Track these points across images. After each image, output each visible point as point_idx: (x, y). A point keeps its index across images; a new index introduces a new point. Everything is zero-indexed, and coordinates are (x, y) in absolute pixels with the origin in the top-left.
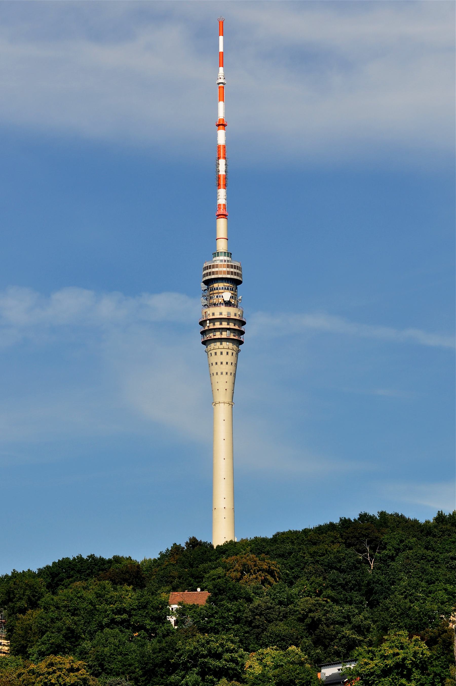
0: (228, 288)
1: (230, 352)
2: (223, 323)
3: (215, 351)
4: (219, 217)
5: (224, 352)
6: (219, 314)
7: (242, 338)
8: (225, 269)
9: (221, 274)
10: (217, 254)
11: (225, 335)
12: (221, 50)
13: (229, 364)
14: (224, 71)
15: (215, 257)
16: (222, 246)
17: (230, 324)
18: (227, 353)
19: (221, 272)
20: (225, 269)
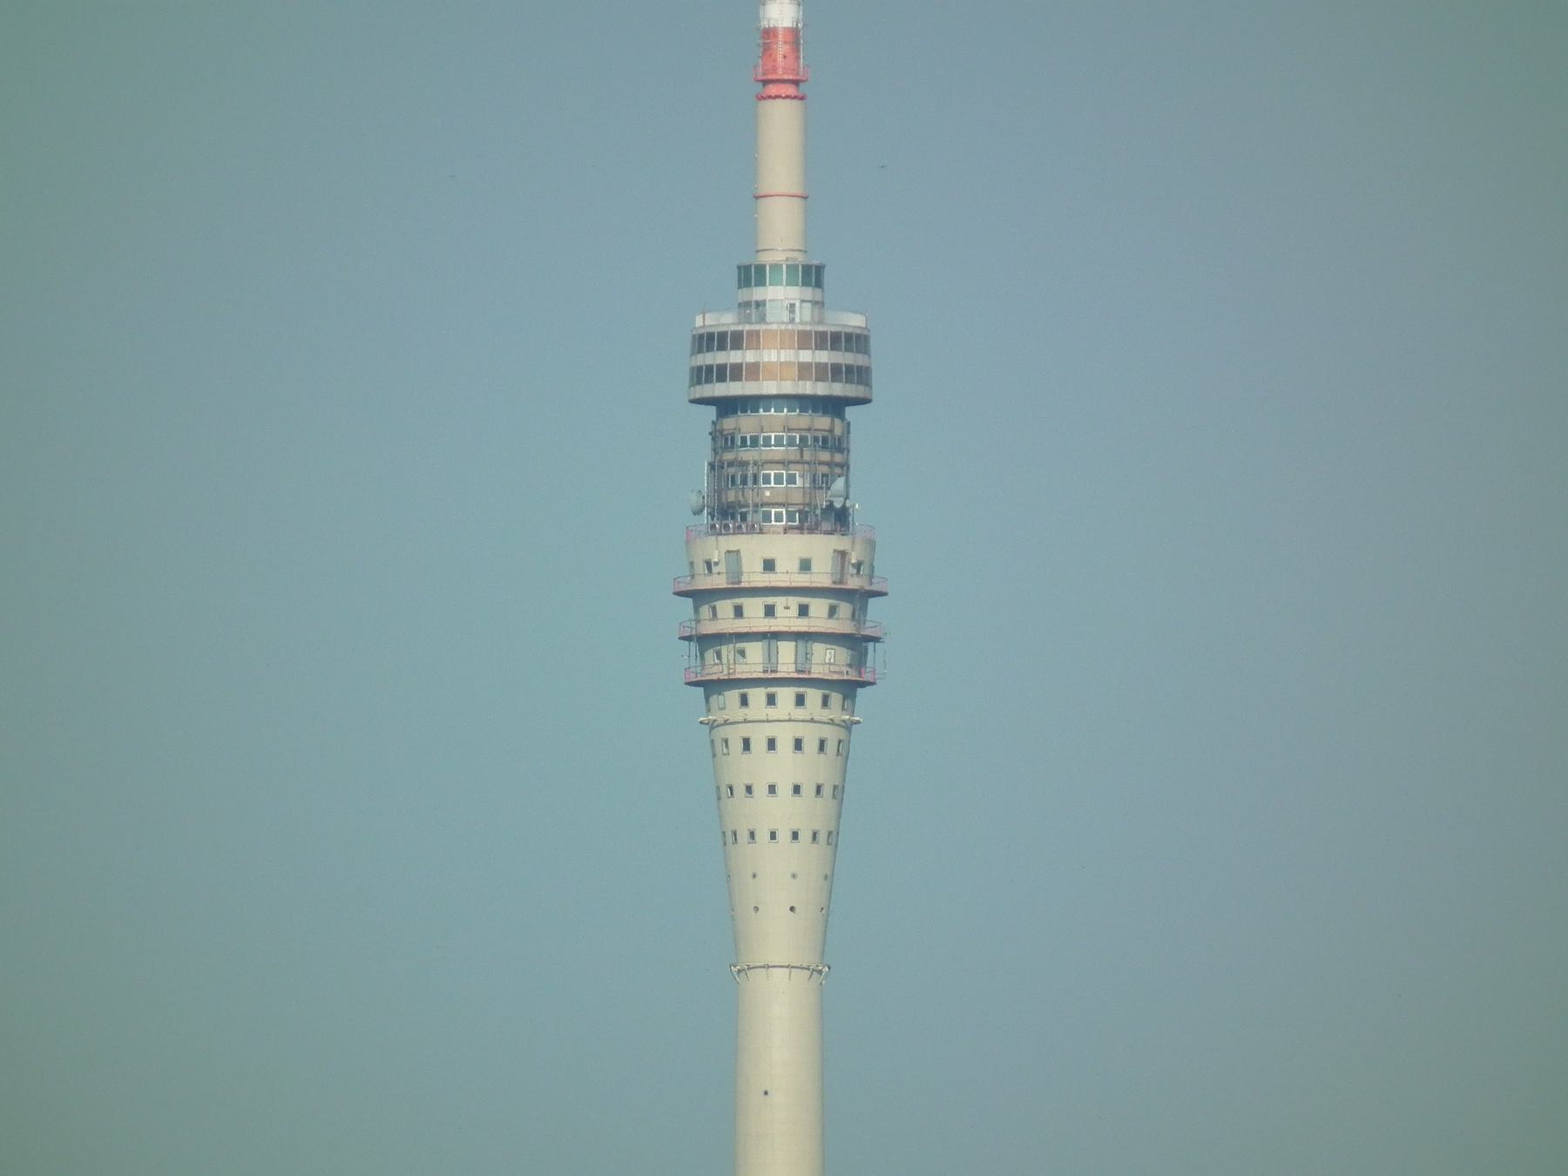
0: (803, 439)
3: (745, 731)
4: (773, 89)
6: (796, 566)
7: (803, 88)
8: (787, 355)
10: (751, 275)
14: (810, 131)
16: (781, 233)
18: (798, 744)
19: (775, 371)
20: (787, 355)
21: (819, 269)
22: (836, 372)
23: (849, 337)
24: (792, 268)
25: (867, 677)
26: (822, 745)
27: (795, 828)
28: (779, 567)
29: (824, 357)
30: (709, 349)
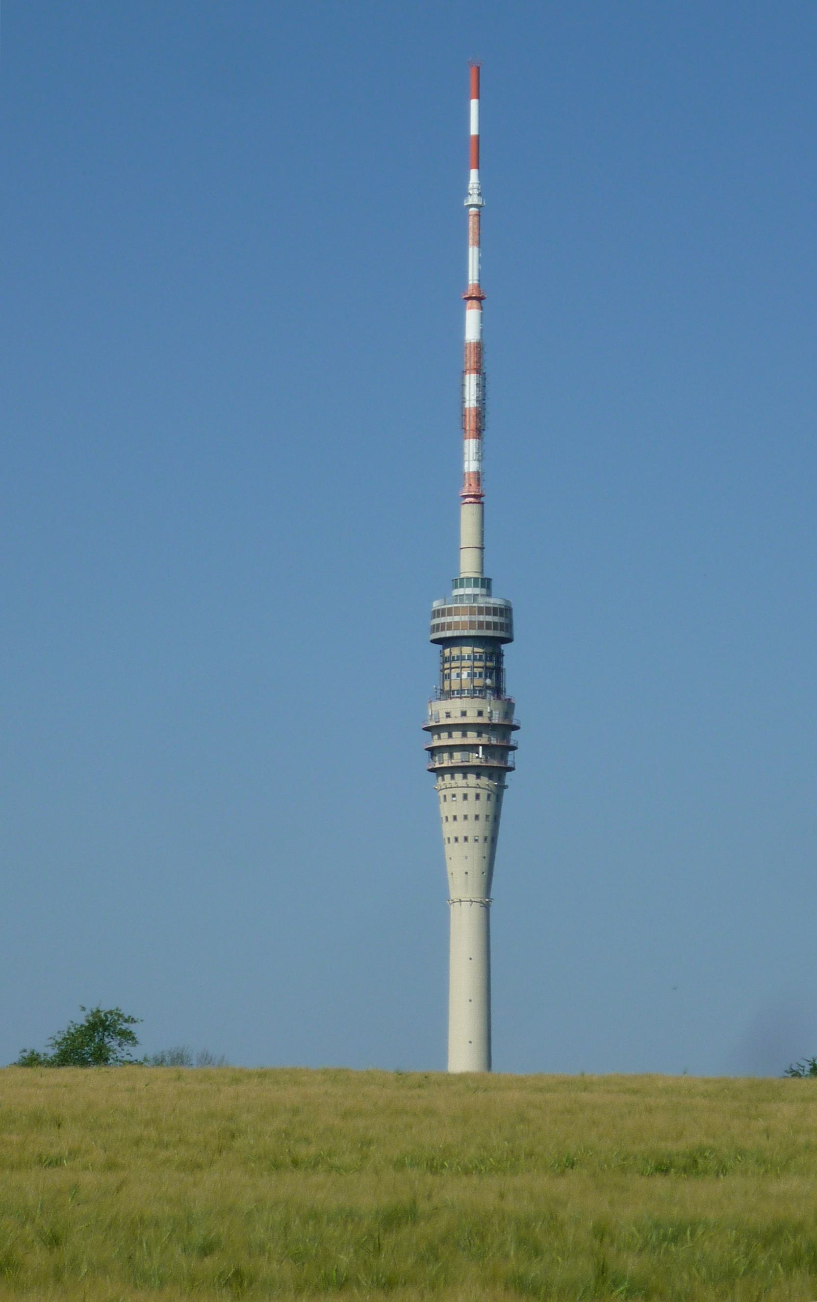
1: (484, 794)
2: (469, 734)
5: (471, 793)
6: (459, 714)
7: (482, 499)
8: (466, 618)
9: (449, 628)
10: (458, 583)
11: (458, 758)
12: (474, 130)
13: (470, 839)
14: (480, 177)
15: (456, 588)
16: (468, 565)
17: (469, 733)
18: (465, 797)
20: (466, 618)
21: (489, 580)
22: (496, 626)
23: (495, 609)
24: (476, 579)
25: (509, 764)
26: (477, 797)
27: (466, 835)
28: (452, 715)
29: (490, 618)
30: (438, 617)
